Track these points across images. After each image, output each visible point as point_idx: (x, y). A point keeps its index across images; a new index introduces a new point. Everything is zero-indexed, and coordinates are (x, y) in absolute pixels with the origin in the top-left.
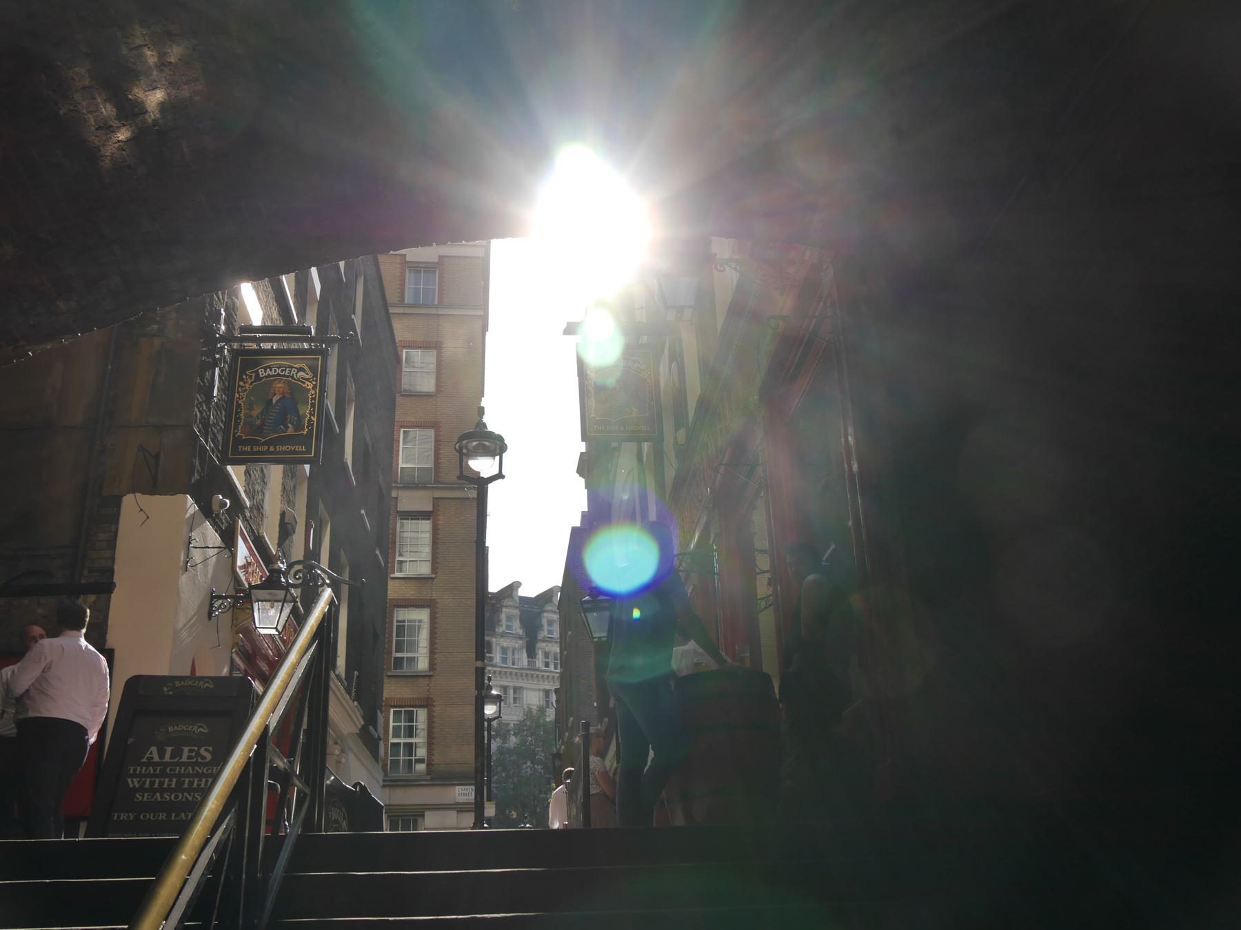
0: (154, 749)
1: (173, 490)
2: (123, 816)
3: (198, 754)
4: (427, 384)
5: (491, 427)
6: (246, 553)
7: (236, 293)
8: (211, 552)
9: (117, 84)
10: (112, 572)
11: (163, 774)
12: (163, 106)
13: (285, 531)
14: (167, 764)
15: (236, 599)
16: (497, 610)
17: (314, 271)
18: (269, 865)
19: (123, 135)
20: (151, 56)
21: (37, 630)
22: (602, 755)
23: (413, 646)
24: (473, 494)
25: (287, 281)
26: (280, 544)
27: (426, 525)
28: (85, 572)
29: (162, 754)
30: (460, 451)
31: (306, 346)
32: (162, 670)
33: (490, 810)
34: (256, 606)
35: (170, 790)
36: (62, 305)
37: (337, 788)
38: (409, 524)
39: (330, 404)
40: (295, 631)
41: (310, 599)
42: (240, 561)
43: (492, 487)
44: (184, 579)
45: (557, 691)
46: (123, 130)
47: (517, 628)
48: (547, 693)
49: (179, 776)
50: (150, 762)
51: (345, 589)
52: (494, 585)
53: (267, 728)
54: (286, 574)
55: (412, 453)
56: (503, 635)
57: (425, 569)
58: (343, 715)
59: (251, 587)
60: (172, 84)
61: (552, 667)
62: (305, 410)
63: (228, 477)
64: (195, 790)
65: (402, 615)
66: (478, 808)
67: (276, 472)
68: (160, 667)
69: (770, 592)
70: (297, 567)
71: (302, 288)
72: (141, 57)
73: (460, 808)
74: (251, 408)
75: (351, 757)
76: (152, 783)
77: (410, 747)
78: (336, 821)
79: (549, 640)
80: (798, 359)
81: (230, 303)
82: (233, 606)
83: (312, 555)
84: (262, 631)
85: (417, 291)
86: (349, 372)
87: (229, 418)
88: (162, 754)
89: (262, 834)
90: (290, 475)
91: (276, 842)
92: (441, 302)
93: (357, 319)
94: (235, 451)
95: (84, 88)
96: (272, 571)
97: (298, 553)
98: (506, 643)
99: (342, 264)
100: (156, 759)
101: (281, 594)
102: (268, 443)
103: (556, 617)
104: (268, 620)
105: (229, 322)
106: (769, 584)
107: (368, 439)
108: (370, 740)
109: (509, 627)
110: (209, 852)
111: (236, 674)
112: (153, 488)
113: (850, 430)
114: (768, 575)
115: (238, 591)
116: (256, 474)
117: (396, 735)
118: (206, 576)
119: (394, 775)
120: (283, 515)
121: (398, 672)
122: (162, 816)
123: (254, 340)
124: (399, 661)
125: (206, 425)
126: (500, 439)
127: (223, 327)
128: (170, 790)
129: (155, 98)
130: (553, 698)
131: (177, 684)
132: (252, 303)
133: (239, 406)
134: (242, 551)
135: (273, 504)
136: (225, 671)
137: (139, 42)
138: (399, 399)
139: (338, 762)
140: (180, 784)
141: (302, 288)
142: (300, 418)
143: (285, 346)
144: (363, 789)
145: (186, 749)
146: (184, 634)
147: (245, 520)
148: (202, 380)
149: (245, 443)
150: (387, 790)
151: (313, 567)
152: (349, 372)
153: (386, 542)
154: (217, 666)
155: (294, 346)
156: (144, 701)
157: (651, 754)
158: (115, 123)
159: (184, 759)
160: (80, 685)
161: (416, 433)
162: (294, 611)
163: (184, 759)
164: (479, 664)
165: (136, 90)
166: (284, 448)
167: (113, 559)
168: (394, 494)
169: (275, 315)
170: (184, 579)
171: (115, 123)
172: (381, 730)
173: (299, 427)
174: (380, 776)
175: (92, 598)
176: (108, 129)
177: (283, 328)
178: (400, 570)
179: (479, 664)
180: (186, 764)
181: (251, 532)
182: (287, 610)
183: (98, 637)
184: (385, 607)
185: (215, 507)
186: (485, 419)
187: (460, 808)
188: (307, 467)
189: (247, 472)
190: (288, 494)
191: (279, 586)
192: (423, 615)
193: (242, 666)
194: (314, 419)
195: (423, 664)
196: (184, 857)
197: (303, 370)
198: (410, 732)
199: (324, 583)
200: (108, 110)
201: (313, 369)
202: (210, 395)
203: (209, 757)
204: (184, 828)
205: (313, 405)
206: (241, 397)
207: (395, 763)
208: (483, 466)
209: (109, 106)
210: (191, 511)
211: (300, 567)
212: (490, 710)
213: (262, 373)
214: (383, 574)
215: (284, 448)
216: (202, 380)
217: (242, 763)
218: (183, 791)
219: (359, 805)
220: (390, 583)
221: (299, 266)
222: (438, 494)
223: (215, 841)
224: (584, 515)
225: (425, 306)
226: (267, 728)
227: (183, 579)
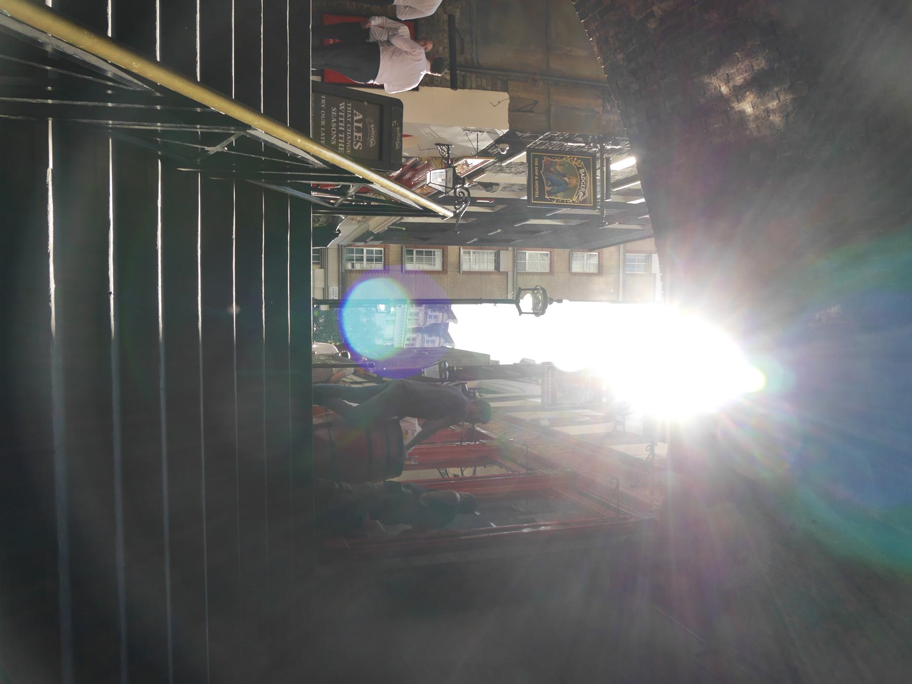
0: (361, 117)
1: (511, 121)
2: (323, 101)
3: (358, 142)
4: (576, 267)
5: (550, 308)
6: (474, 164)
7: (630, 153)
8: (475, 144)
9: (759, 84)
10: (463, 88)
11: (347, 122)
12: (742, 112)
13: (487, 186)
14: (352, 125)
15: (447, 159)
16: (440, 310)
17: (643, 200)
18: (294, 186)
19: (724, 89)
20: (773, 104)
21: (430, 46)
22: (355, 373)
23: (420, 260)
24: (510, 297)
25: (637, 184)
26: (480, 183)
27: (491, 268)
28: (463, 73)
29: (357, 121)
31: (599, 196)
32: (406, 119)
33: (324, 308)
34: (444, 170)
35: (338, 126)
36: (620, 56)
37: (336, 222)
38: (492, 257)
40: (425, 195)
41: (444, 201)
42: (470, 161)
43: (514, 306)
45: (393, 345)
46: (727, 90)
47: (431, 321)
48: (392, 339)
49: (345, 132)
50: (353, 115)
51: (454, 221)
52: (455, 308)
53: (372, 183)
54: (462, 187)
55: (535, 259)
56: (426, 313)
57: (465, 267)
58: (378, 223)
59: (454, 168)
60: (757, 118)
61: (407, 342)
62: (560, 197)
63: (519, 152)
64: (337, 141)
65: (438, 253)
66: (324, 302)
67: (523, 180)
68: (408, 117)
69: (451, 476)
70: (466, 193)
71: (634, 193)
72: (773, 99)
73: (325, 290)
74: (560, 165)
75: (356, 226)
76: (342, 116)
77: (360, 260)
78: (319, 220)
79: (423, 341)
80: (675, 445)
82: (443, 157)
83: (474, 201)
84: (428, 175)
87: (555, 152)
88: (357, 121)
89: (312, 182)
90: (521, 188)
91: (307, 189)
93: (616, 226)
94: (535, 156)
95: (752, 66)
96: (463, 179)
97: (474, 193)
98: (421, 315)
99: (648, 216)
100: (355, 118)
101: (450, 185)
102: (540, 175)
103: (437, 345)
104: (436, 178)
106: (455, 476)
108: (364, 237)
109: (430, 317)
110: (302, 154)
111: (403, 160)
112: (512, 110)
113: (549, 528)
114: (460, 475)
115: (452, 160)
116: (521, 169)
118: (352, 383)
119: (345, 251)
120: (497, 184)
122: (323, 123)
123: (602, 166)
124: (411, 252)
125: (551, 139)
126: (543, 313)
127: (609, 147)
128: (338, 126)
129: (747, 106)
130: (389, 344)
131: (398, 128)
132: (624, 164)
133: (562, 158)
134: (475, 162)
135: (502, 178)
136: (405, 154)
137: (782, 97)
138: (567, 251)
139: (353, 219)
140: (341, 132)
141: (634, 193)
142: (555, 194)
143: (598, 184)
144: (337, 235)
145: (360, 135)
146: (427, 130)
147: (494, 163)
149: (540, 162)
150: (336, 247)
151: (466, 203)
153: (483, 243)
154: (409, 149)
155: (598, 189)
156: (389, 111)
157: (355, 405)
158: (731, 84)
159: (355, 134)
160: (400, 74)
161: (547, 262)
162: (440, 192)
163: (355, 134)
165: (752, 96)
167: (471, 88)
168: (510, 249)
169: (617, 178)
171: (731, 84)
172: (371, 243)
173: (550, 193)
174: (344, 243)
175: (448, 77)
176: (728, 80)
177: (610, 183)
178: (464, 253)
180: (352, 135)
181: (487, 167)
182: (440, 189)
183: (428, 81)
184: (442, 245)
185: (501, 146)
186: (555, 303)
187: (325, 290)
188: (526, 198)
189: (522, 163)
190: (509, 187)
191: (455, 183)
192: (438, 266)
193: (408, 163)
194: (554, 202)
195: (409, 266)
196: (299, 141)
198: (370, 260)
199: (457, 209)
200: (739, 80)
201: (584, 201)
202: (568, 141)
203: (356, 148)
204: (316, 140)
205: (563, 201)
206: (567, 159)
207: (352, 251)
208: (527, 302)
209: (742, 81)
210: (499, 132)
211: (466, 195)
212: (382, 307)
213: (582, 171)
214: (462, 242)
217: (352, 170)
219: (329, 232)
220: (457, 247)
221: (649, 189)
222: (510, 274)
223: (308, 157)
224: (497, 362)
225: (624, 265)
226: (372, 183)
227: (458, 127)
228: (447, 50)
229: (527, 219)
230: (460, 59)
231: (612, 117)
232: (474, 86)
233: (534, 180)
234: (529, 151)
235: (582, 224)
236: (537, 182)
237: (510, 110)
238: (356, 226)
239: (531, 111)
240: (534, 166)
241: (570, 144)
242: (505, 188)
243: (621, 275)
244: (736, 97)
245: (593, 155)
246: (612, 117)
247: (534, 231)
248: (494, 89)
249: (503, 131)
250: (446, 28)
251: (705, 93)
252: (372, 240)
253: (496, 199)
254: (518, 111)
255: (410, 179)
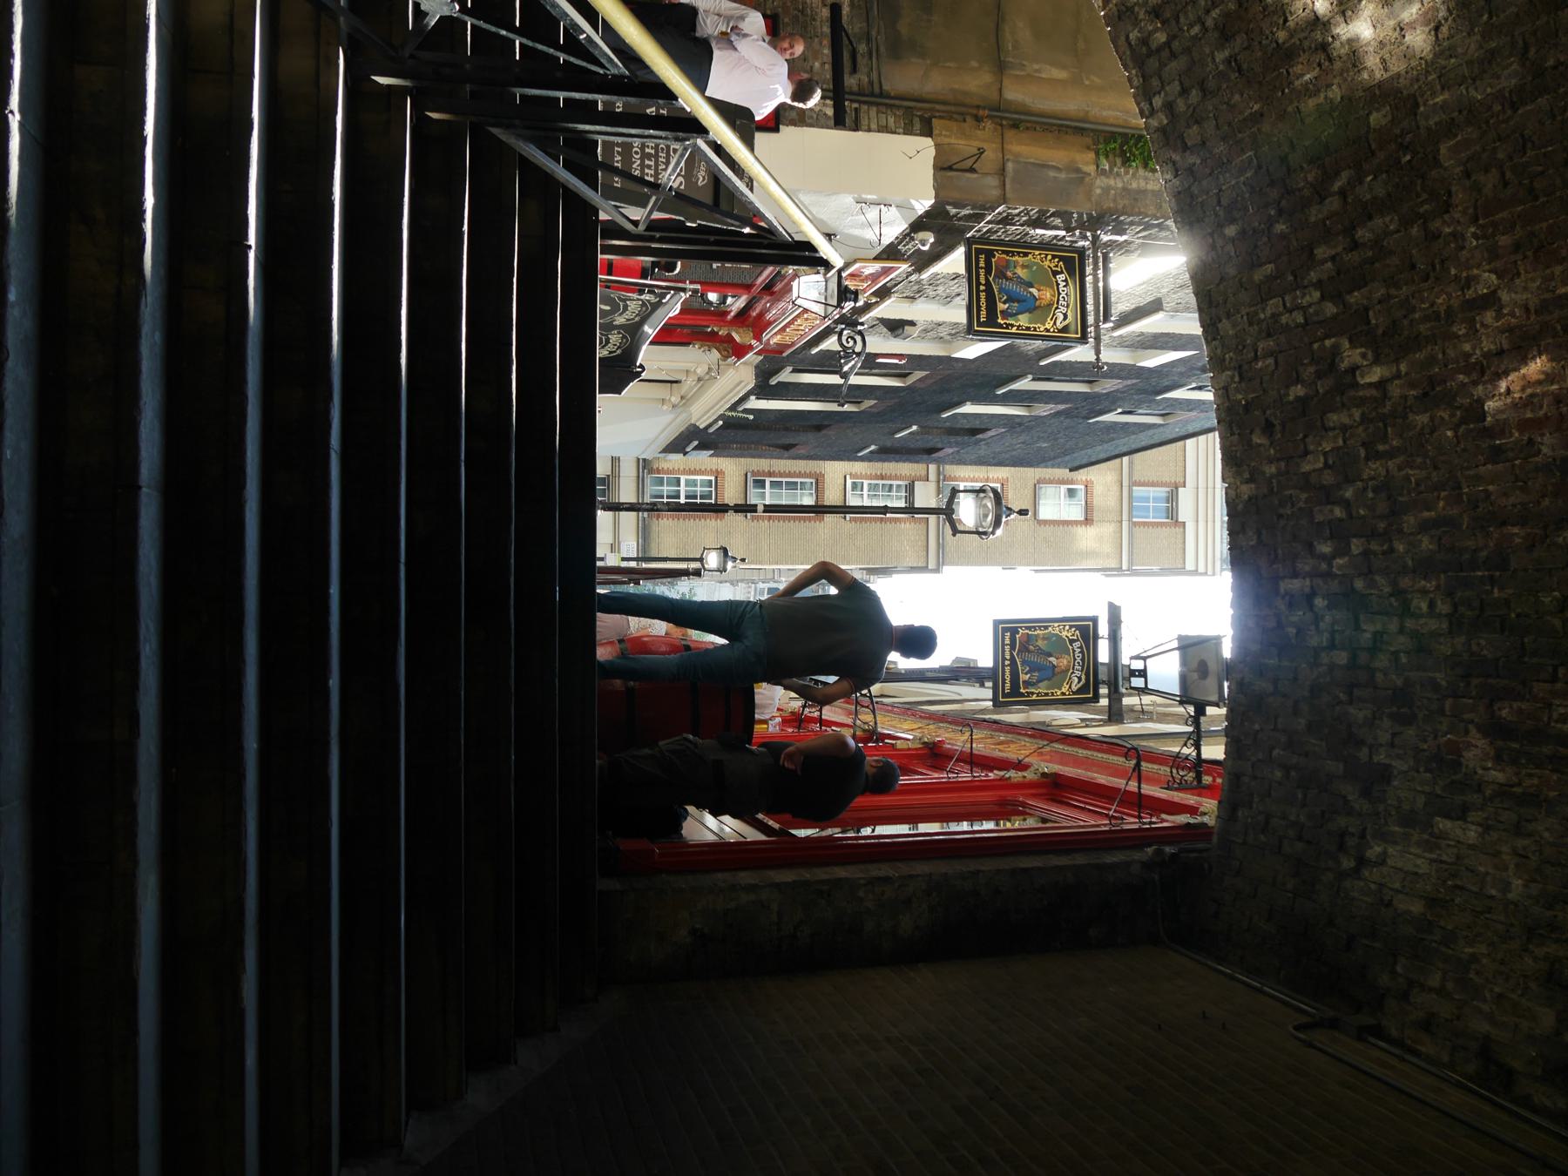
1: (938, 187)
12: (1352, 41)
13: (896, 327)
21: (799, 49)
28: (855, 105)
30: (982, 490)
39: (1025, 384)
44: (849, 200)
49: (656, 156)
62: (1023, 320)
64: (642, 171)
74: (1023, 267)
75: (670, 417)
81: (1133, 247)
85: (1147, 499)
86: (1061, 407)
92: (1135, 524)
94: (979, 252)
102: (988, 284)
105: (1111, 244)
107: (990, 433)
117: (688, 483)
120: (912, 323)
121: (750, 483)
123: (1096, 268)
125: (1006, 220)
133: (1026, 255)
135: (922, 312)
140: (649, 156)
148: (1053, 215)
152: (1061, 407)
164: (761, 508)
166: (983, 300)
167: (869, 130)
170: (849, 200)
173: (1005, 314)
179: (761, 508)
189: (957, 276)
197: (1065, 317)
201: (1065, 329)
205: (1028, 329)
206: (1036, 257)
213: (1061, 277)
215: (983, 300)
216: (1053, 215)
218: (642, 159)
228: (827, 66)
229: (960, 403)
230: (850, 82)
231: (1112, 182)
232: (874, 126)
233: (978, 267)
234: (969, 243)
235: (1058, 414)
236: (983, 295)
237: (935, 167)
238: (670, 417)
239: (972, 170)
240: (978, 267)
241: (1039, 231)
242: (926, 331)
243: (1125, 524)
244: (1343, 13)
245: (1081, 252)
246: (1112, 182)
247: (974, 430)
248: (908, 131)
249: (923, 205)
250: (827, 30)
251: (1286, 21)
252: (695, 448)
253: (910, 357)
254: (950, 168)
255: (761, 315)
